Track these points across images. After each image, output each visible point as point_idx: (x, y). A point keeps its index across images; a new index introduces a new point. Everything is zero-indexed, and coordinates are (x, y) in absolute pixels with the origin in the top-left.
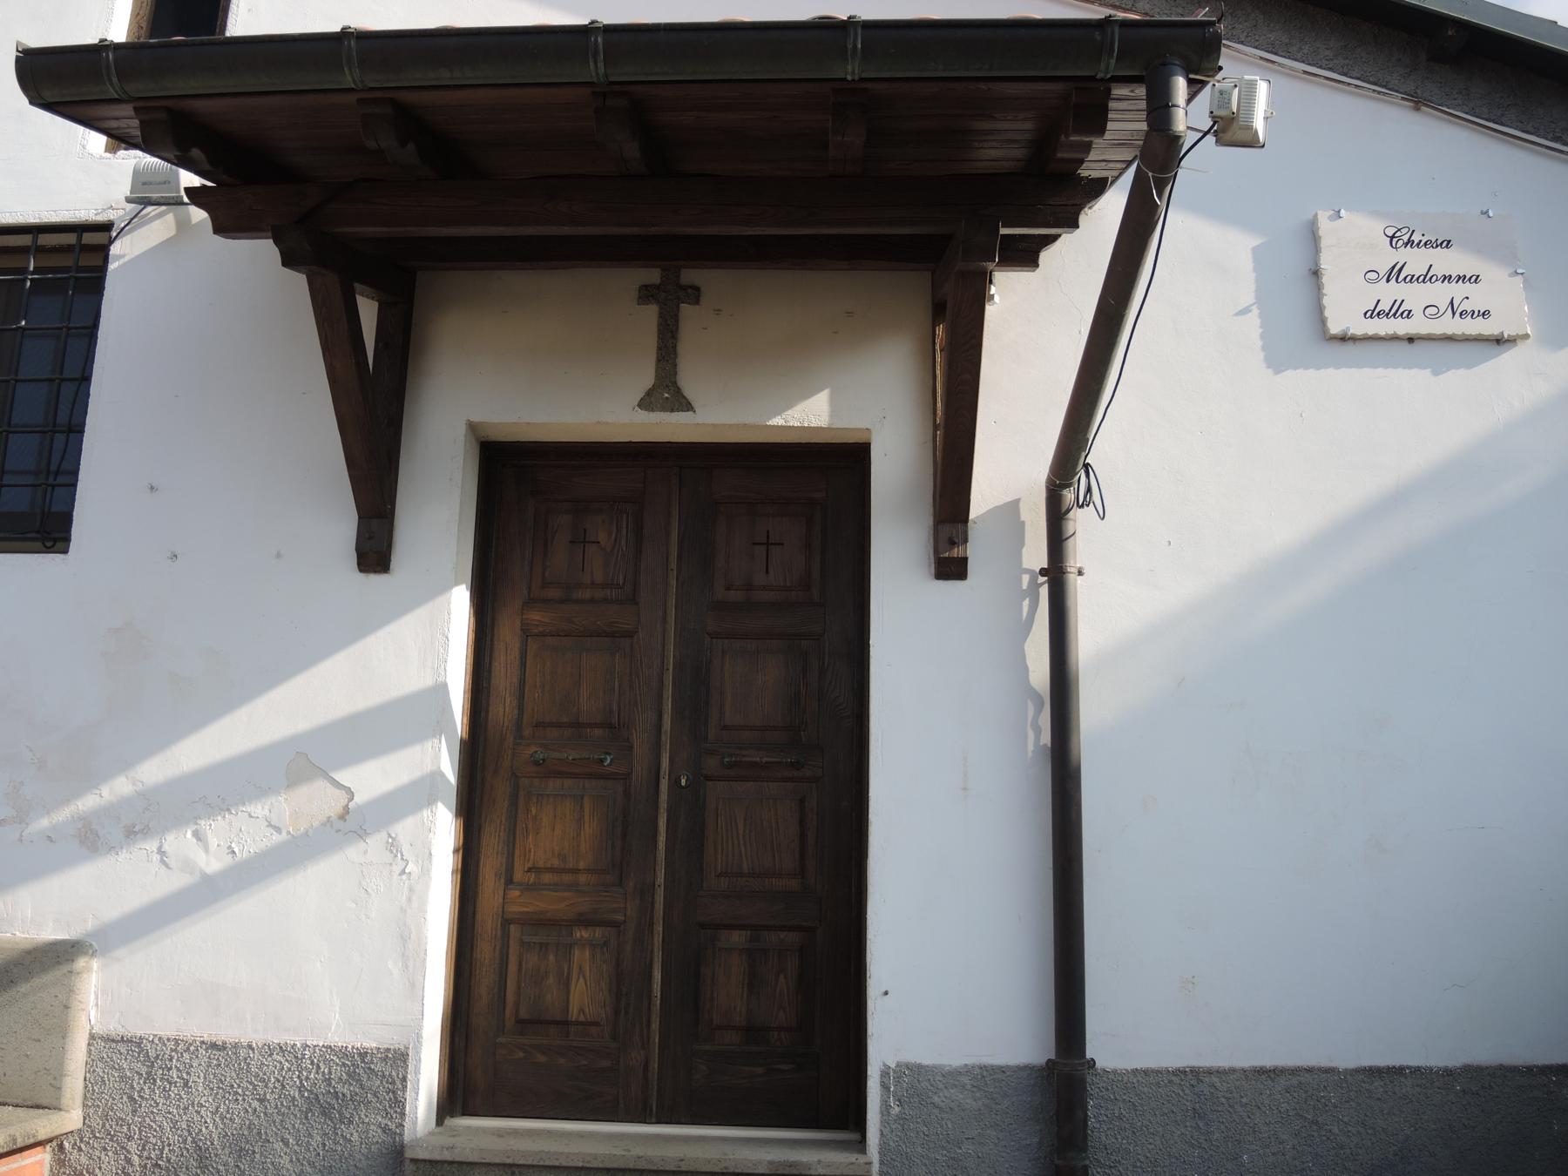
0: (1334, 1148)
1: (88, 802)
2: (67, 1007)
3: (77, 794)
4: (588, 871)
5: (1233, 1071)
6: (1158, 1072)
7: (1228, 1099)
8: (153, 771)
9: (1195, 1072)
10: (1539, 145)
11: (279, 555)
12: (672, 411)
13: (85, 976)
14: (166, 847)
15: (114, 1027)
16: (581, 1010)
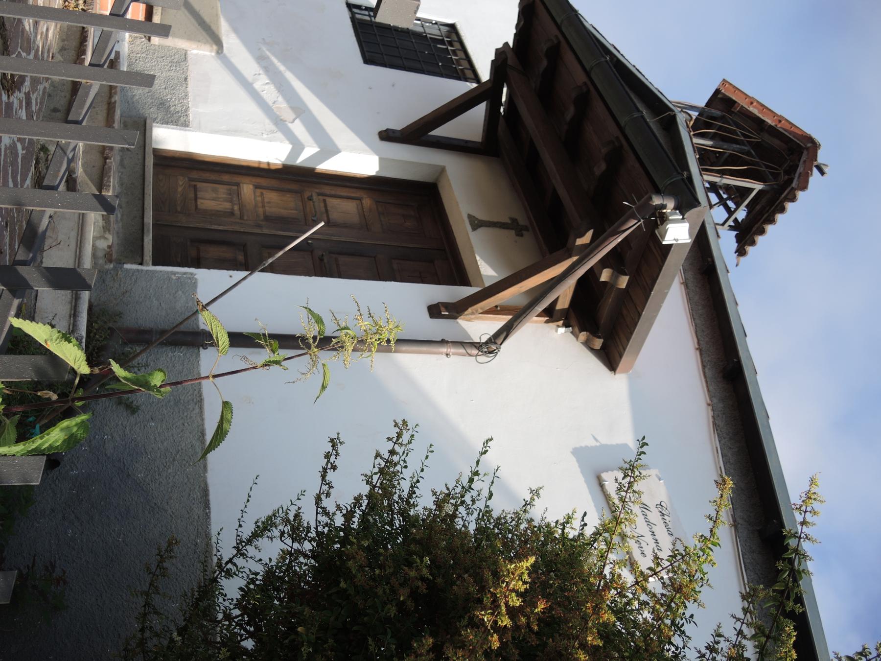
0: (159, 469)
1: (275, 60)
2: (199, 41)
3: (276, 57)
4: (264, 213)
5: (203, 420)
7: (187, 417)
8: (289, 76)
10: (741, 564)
11: (378, 113)
12: (470, 224)
14: (261, 76)
15: (189, 57)
16: (202, 203)
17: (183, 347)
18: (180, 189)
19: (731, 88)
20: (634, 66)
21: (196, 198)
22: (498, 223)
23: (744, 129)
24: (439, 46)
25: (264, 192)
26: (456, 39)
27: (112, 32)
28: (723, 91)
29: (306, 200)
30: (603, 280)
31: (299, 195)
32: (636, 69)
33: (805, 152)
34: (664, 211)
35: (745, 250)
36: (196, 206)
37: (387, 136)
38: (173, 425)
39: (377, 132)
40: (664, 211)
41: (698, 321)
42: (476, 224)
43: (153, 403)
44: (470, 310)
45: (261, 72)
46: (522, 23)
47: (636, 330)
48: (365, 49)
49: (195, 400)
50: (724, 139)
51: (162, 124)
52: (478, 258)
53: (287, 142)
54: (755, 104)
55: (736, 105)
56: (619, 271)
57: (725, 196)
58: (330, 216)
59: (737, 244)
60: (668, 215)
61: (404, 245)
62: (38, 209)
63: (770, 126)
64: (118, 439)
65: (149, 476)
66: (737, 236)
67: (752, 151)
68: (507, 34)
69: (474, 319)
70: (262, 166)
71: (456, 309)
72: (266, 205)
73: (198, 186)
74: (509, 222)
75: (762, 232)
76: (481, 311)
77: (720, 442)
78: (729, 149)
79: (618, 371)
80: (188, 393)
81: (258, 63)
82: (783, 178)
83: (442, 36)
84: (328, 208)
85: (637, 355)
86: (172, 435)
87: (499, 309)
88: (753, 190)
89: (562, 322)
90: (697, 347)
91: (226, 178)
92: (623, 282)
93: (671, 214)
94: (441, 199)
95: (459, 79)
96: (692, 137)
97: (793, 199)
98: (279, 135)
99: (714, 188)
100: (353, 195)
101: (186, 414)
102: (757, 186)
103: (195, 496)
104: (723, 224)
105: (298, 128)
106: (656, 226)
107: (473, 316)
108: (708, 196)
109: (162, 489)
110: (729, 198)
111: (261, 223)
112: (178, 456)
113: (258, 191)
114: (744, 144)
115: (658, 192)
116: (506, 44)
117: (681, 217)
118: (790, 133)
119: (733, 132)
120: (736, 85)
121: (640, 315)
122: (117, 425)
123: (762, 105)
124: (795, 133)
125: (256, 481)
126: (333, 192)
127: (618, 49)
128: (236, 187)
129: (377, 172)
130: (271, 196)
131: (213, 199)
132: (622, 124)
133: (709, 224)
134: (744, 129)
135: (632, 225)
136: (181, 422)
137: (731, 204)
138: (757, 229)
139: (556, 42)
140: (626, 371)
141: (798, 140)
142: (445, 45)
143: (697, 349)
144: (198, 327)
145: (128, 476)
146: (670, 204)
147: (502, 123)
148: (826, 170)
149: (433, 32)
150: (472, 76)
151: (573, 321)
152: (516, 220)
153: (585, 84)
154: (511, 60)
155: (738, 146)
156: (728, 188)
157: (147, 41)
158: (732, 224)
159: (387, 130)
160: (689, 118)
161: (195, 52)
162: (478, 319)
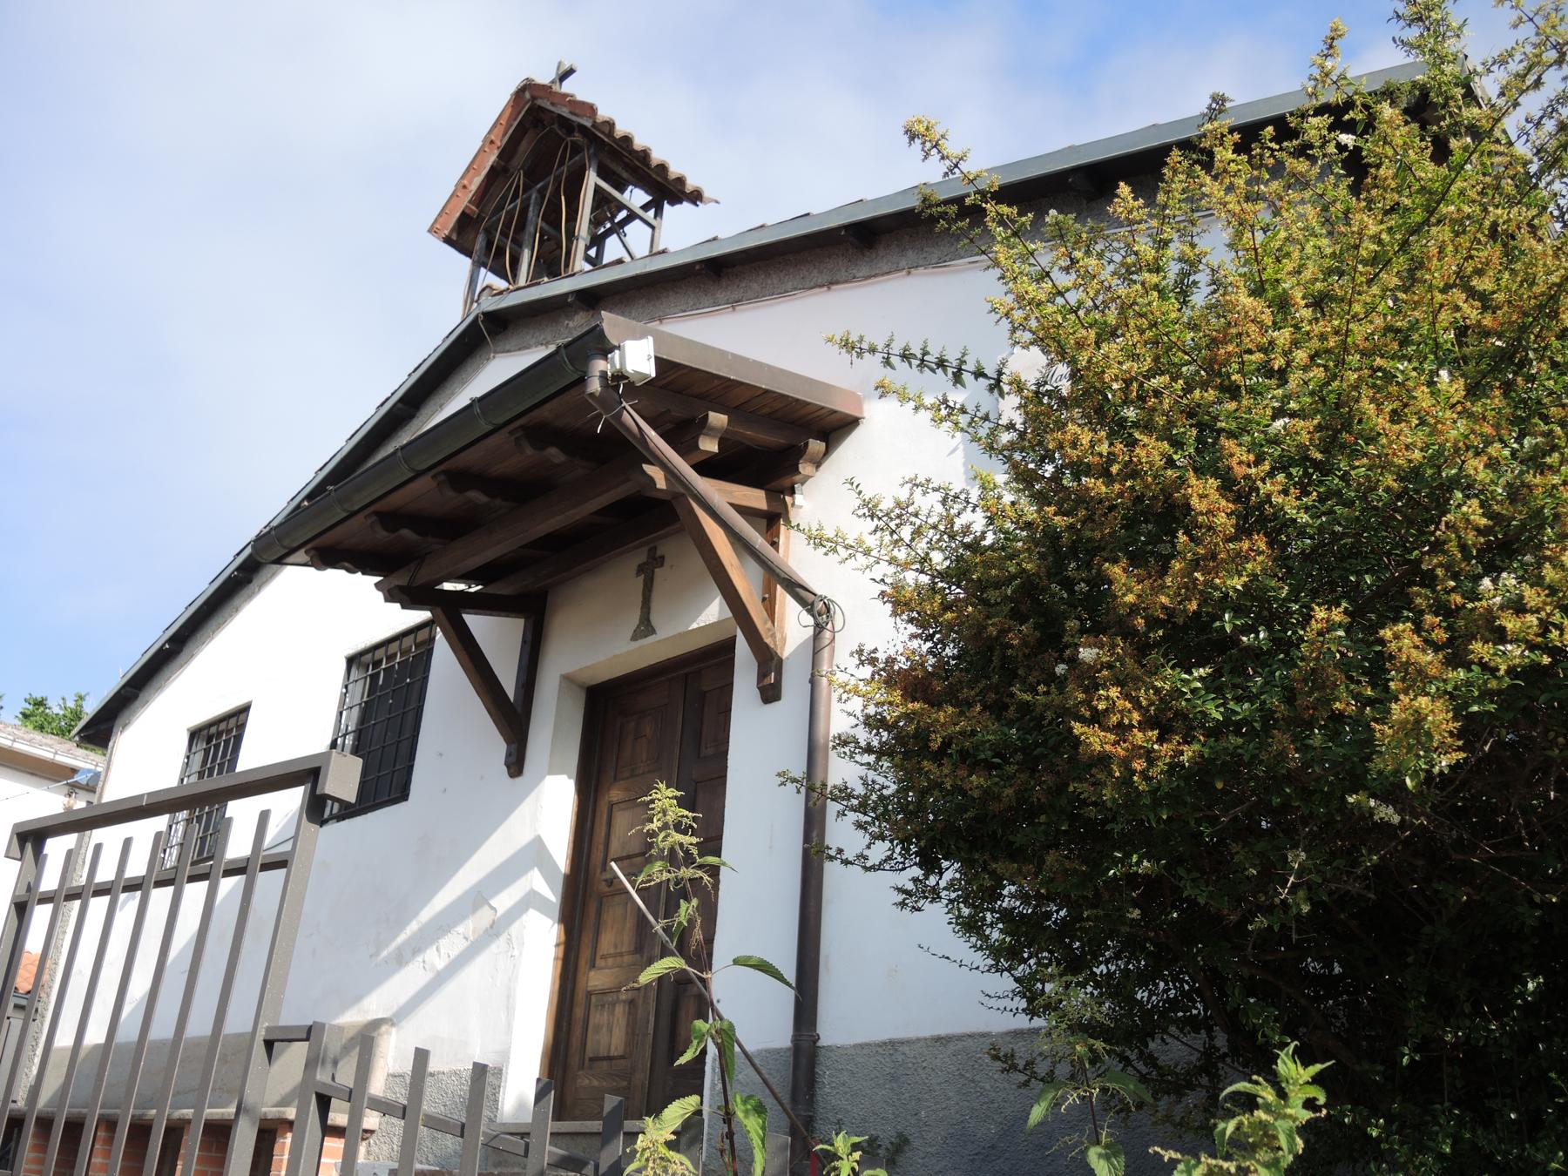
4: (630, 953)
5: (918, 1040)
6: (868, 1045)
8: (426, 915)
9: (893, 1044)
11: (482, 778)
12: (646, 637)
13: (385, 1037)
14: (426, 959)
16: (616, 1049)
17: (817, 1070)
18: (595, 1083)
19: (441, 220)
20: (410, 375)
21: (609, 1058)
22: (644, 594)
23: (505, 198)
24: (381, 682)
25: (600, 953)
26: (370, 655)
27: (369, 1098)
28: (447, 232)
29: (611, 889)
30: (716, 447)
31: (605, 899)
32: (414, 372)
33: (539, 102)
34: (609, 374)
35: (692, 192)
36: (622, 1057)
37: (516, 765)
38: (925, 1084)
39: (511, 780)
40: (609, 374)
41: (789, 286)
42: (645, 627)
43: (894, 1114)
44: (768, 641)
45: (420, 959)
46: (346, 564)
47: (791, 395)
48: (387, 798)
49: (891, 1052)
50: (521, 226)
51: (497, 1109)
52: (694, 626)
53: (524, 917)
54: (465, 182)
55: (467, 211)
56: (702, 426)
57: (608, 225)
58: (637, 852)
59: (685, 203)
60: (614, 370)
61: (678, 739)
62: (546, 1159)
63: (500, 156)
64: (943, 1163)
65: (995, 1117)
66: (672, 203)
67: (539, 186)
68: (365, 584)
69: (782, 633)
70: (561, 955)
71: (768, 661)
72: (618, 951)
73: (591, 1055)
74: (642, 578)
75: (663, 168)
76: (769, 623)
77: (962, 258)
78: (536, 221)
79: (857, 415)
80: (881, 1062)
81: (407, 963)
82: (577, 137)
83: (366, 678)
84: (624, 854)
85: (833, 386)
86: (939, 1084)
87: (767, 596)
88: (596, 185)
89: (788, 499)
90: (825, 289)
91: (579, 1012)
92: (718, 419)
93: (613, 365)
94: (603, 683)
95: (430, 652)
96: (516, 286)
97: (610, 125)
98: (514, 929)
99: (598, 241)
100: (605, 817)
101: (910, 1065)
102: (592, 179)
103: (1023, 1049)
104: (653, 228)
105: (504, 901)
106: (630, 386)
107: (778, 636)
108: (605, 266)
109: (1012, 1098)
110: (611, 220)
111: (645, 958)
112: (968, 1075)
113: (599, 962)
114: (529, 198)
115: (582, 381)
116: (377, 585)
117: (617, 352)
118: (509, 125)
119: (511, 214)
120: (437, 213)
121: (767, 391)
122: (923, 1165)
123: (468, 170)
124: (509, 117)
125: (926, 948)
126: (601, 847)
127: (383, 400)
128: (593, 997)
129: (570, 778)
130: (607, 942)
131: (610, 1031)
132: (490, 427)
133: (646, 265)
134: (505, 198)
135: (631, 418)
136: (921, 1071)
137: (623, 214)
138: (658, 175)
139: (374, 518)
140: (859, 402)
141: (520, 113)
142: (379, 673)
143: (829, 288)
144: (789, 1049)
145: (993, 1147)
146: (600, 365)
147: (495, 589)
148: (566, 66)
149: (358, 692)
150: (427, 630)
151: (786, 482)
152: (639, 566)
153: (434, 477)
154: (401, 579)
155: (531, 209)
156: (596, 222)
157: (374, 1136)
158: (652, 213)
159: (508, 765)
160: (487, 291)
161: (390, 1062)
162: (782, 628)
